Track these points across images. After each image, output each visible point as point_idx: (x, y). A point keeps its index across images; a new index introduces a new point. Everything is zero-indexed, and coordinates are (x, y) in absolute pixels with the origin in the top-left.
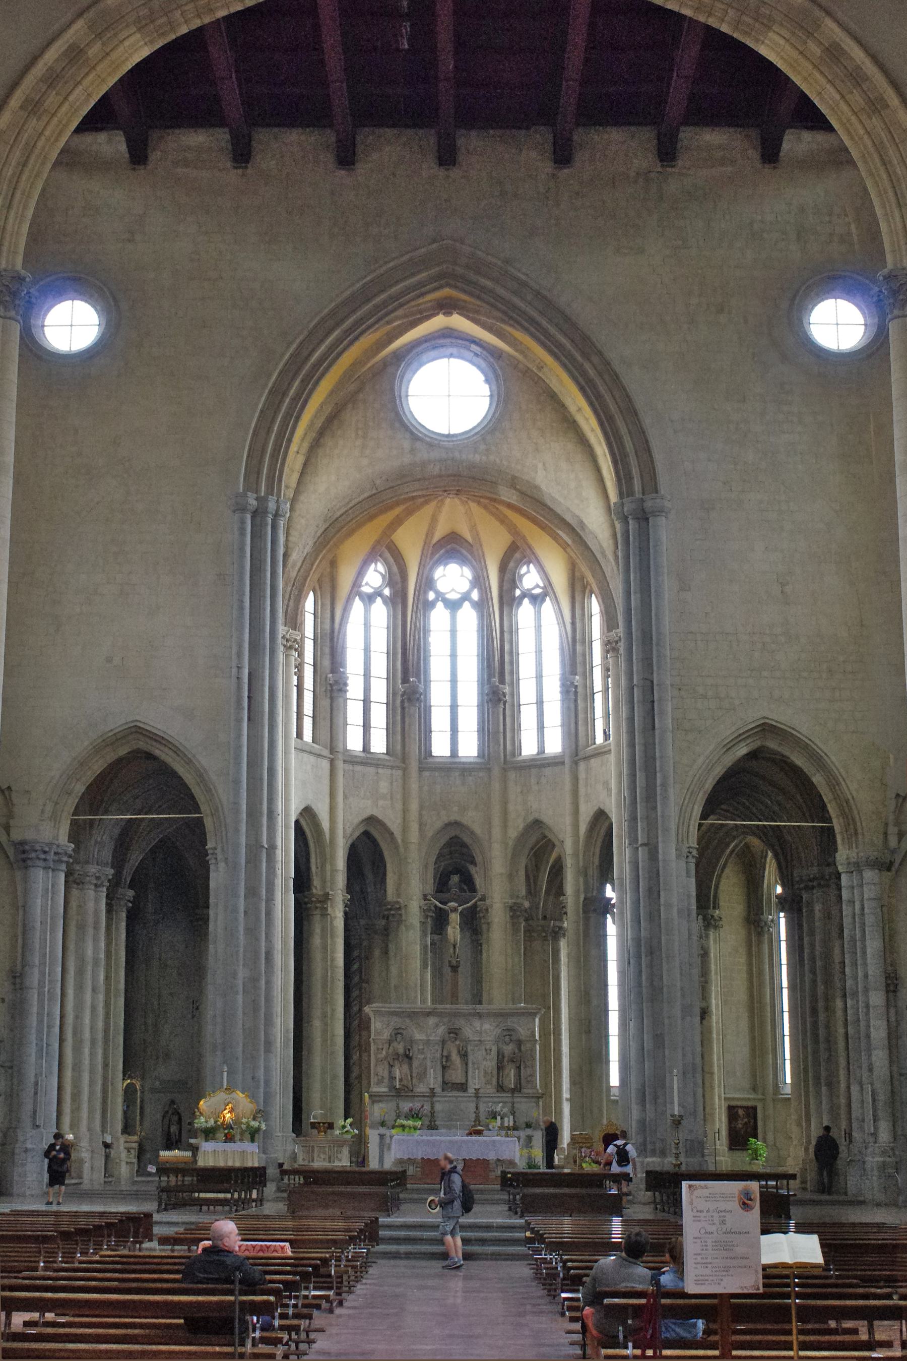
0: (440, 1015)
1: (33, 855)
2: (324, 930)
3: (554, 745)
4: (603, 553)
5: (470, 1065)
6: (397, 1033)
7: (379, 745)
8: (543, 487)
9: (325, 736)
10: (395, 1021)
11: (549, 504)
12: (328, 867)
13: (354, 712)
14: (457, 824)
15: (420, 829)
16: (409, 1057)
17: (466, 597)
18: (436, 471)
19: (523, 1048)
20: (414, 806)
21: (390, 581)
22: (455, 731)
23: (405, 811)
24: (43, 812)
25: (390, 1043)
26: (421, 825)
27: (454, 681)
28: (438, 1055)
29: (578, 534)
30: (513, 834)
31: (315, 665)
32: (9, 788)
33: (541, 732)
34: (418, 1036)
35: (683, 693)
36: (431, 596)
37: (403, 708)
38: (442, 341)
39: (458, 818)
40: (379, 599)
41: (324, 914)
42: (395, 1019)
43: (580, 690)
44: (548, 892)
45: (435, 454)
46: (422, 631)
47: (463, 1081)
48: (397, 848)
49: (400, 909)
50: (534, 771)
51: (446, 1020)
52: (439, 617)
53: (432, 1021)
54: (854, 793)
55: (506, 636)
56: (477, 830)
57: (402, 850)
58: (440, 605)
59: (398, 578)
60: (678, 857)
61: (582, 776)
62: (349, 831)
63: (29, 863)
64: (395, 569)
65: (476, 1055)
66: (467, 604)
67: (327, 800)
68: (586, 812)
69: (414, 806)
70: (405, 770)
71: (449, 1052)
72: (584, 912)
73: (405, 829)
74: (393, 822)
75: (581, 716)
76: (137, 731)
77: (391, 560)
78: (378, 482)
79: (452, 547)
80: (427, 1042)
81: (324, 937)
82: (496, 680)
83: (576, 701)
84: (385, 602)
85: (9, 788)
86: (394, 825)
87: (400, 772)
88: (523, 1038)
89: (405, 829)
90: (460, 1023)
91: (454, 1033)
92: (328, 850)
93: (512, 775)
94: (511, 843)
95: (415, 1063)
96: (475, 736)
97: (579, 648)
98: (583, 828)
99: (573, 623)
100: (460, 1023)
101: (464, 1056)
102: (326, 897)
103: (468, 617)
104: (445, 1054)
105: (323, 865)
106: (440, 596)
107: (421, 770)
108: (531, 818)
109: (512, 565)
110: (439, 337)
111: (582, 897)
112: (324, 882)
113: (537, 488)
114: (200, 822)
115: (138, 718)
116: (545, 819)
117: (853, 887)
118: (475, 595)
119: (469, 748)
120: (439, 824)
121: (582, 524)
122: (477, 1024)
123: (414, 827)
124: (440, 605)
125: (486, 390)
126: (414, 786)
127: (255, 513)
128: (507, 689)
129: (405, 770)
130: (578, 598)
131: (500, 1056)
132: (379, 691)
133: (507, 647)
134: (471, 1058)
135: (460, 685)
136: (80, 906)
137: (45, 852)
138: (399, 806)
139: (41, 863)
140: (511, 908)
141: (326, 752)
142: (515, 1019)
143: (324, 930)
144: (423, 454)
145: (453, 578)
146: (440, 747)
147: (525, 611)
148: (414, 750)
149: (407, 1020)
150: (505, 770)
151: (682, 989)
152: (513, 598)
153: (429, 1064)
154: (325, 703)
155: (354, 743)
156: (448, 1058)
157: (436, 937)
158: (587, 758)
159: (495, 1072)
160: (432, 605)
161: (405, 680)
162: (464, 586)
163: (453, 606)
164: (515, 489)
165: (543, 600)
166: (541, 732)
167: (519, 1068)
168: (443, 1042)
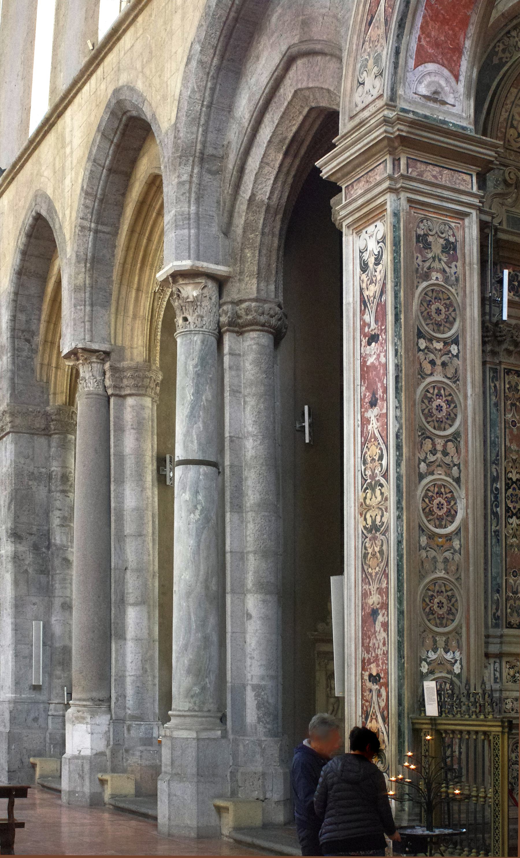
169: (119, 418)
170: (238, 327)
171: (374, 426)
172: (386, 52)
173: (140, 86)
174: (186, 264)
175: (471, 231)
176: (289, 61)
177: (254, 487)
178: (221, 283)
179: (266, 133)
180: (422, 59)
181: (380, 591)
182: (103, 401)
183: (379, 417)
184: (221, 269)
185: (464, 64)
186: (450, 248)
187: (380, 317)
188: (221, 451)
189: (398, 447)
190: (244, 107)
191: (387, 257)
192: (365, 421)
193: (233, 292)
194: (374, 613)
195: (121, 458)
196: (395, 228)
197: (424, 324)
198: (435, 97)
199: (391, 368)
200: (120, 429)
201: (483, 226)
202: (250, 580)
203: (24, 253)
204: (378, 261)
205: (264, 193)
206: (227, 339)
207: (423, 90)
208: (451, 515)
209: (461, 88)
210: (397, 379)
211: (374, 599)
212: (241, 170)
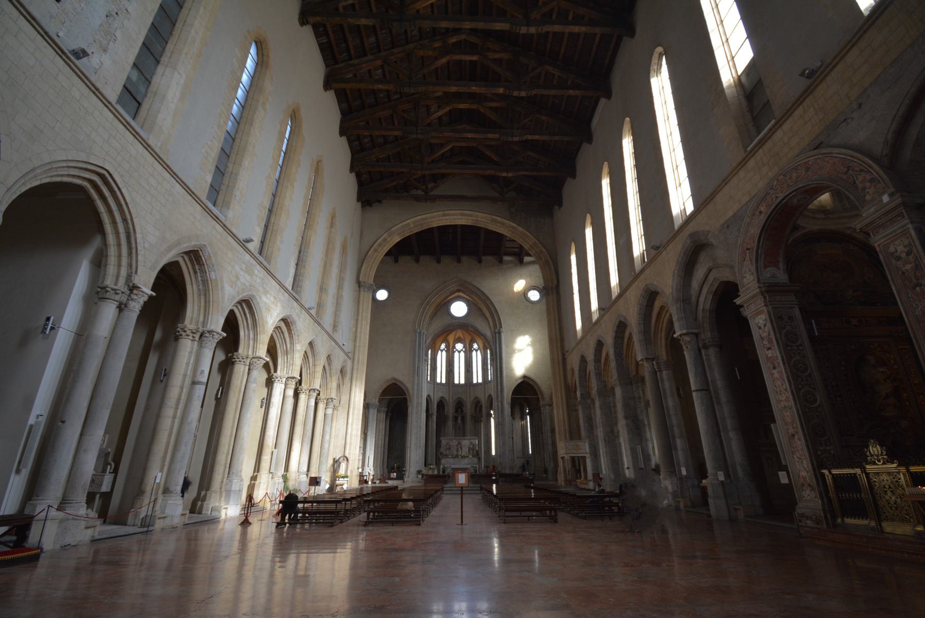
6: (447, 444)
22: (459, 378)
52: (456, 354)
74: (446, 397)
79: (459, 340)
91: (459, 443)
103: (462, 354)
119: (463, 382)
145: (459, 346)
146: (456, 382)
163: (459, 352)
166: (478, 378)
169: (661, 378)
170: (706, 347)
171: (776, 375)
172: (753, 269)
173: (655, 283)
174: (685, 331)
175: (797, 312)
176: (710, 270)
177: (723, 397)
178: (697, 335)
179: (705, 291)
180: (766, 267)
181: (793, 428)
182: (654, 373)
183: (778, 372)
184: (696, 331)
185: (781, 265)
186: (791, 318)
187: (770, 341)
188: (708, 384)
189: (789, 381)
190: (695, 284)
191: (769, 325)
192: (772, 374)
193: (702, 336)
194: (793, 435)
195: (664, 390)
196: (770, 316)
197: (788, 343)
198: (773, 276)
199: (779, 357)
200: (662, 381)
201: (800, 308)
202: (729, 427)
203: (616, 332)
204: (765, 325)
205: (708, 307)
206: (703, 351)
207: (768, 275)
208: (816, 401)
209: (781, 271)
210: (783, 360)
211: (791, 431)
212: (698, 301)
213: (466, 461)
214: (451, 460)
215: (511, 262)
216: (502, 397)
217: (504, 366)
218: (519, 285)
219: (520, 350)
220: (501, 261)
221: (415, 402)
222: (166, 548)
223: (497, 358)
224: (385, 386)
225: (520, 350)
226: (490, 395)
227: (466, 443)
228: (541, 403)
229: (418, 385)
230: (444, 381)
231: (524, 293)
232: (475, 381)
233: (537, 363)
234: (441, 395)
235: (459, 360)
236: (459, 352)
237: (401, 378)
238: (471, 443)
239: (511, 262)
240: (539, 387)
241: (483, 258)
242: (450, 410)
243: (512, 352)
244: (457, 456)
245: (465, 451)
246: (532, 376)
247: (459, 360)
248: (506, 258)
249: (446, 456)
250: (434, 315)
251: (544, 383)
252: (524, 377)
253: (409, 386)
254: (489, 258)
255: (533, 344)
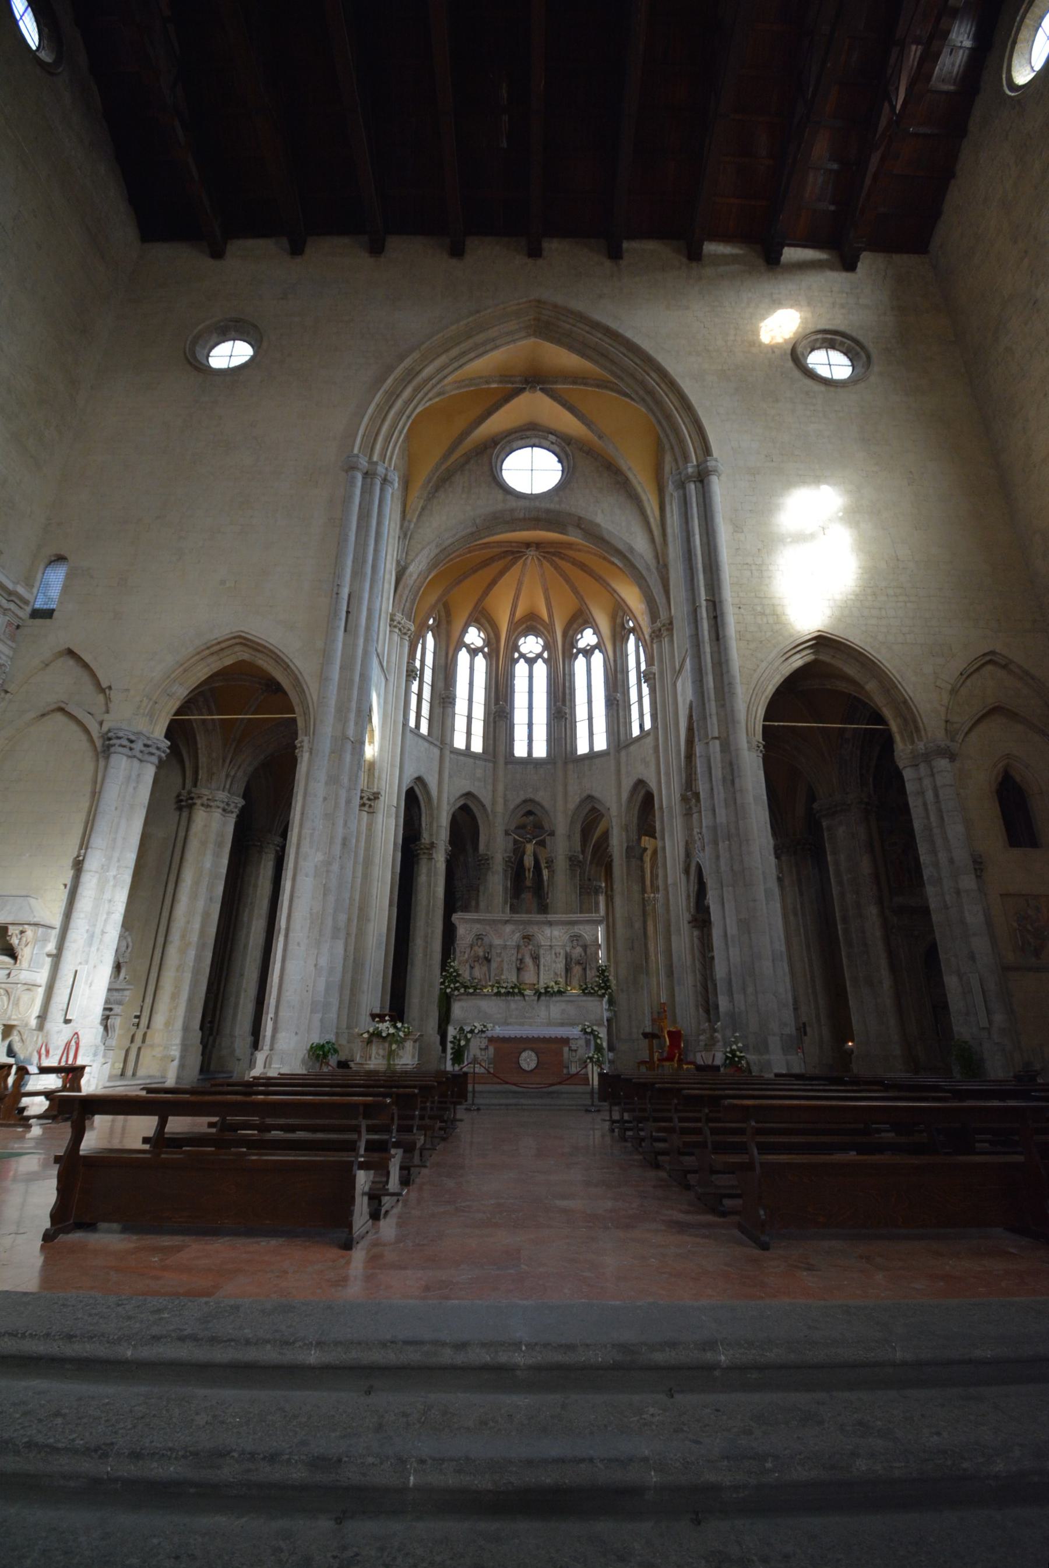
0: (516, 922)
1: (118, 742)
2: (429, 870)
3: (601, 744)
4: (648, 569)
5: (542, 967)
6: (479, 937)
7: (477, 746)
8: (602, 524)
9: (437, 732)
10: (477, 928)
11: (607, 537)
12: (435, 825)
13: (460, 723)
14: (531, 801)
15: (505, 804)
16: (488, 960)
17: (540, 656)
18: (522, 515)
19: (588, 952)
20: (501, 788)
21: (488, 642)
22: (530, 739)
23: (494, 791)
24: (139, 707)
25: (471, 946)
26: (506, 801)
27: (530, 725)
28: (514, 958)
29: (628, 560)
30: (572, 806)
31: (432, 686)
32: (110, 688)
33: (591, 735)
34: (497, 942)
35: (742, 610)
36: (516, 655)
37: (495, 722)
38: (528, 433)
39: (532, 796)
40: (480, 654)
41: (431, 859)
42: (478, 926)
43: (621, 703)
44: (591, 863)
45: (522, 503)
46: (510, 676)
47: (535, 982)
48: (487, 817)
49: (487, 859)
50: (587, 762)
51: (521, 927)
52: (521, 669)
53: (509, 928)
54: (911, 694)
55: (567, 677)
56: (546, 804)
57: (491, 818)
58: (522, 660)
59: (494, 641)
60: (749, 749)
61: (623, 759)
62: (452, 800)
63: (112, 749)
64: (492, 635)
65: (546, 959)
66: (540, 661)
67: (436, 776)
68: (627, 784)
69: (501, 788)
70: (495, 763)
71: (523, 955)
72: (627, 857)
73: (494, 803)
74: (485, 797)
75: (622, 720)
76: (244, 641)
77: (489, 629)
78: (478, 521)
79: (530, 624)
80: (505, 947)
81: (429, 875)
82: (559, 704)
83: (618, 710)
84: (485, 657)
85: (110, 688)
86: (486, 800)
87: (491, 765)
88: (589, 943)
89: (494, 803)
90: (533, 930)
91: (528, 938)
92: (435, 812)
93: (571, 766)
94: (570, 813)
95: (494, 965)
96: (545, 744)
97: (619, 676)
98: (625, 796)
99: (615, 661)
100: (533, 930)
101: (536, 958)
102: (432, 845)
103: (541, 669)
104: (520, 957)
105: (431, 823)
106: (522, 656)
107: (506, 763)
108: (585, 795)
109: (571, 632)
110: (528, 429)
111: (625, 846)
112: (431, 835)
113: (598, 525)
114: (294, 720)
115: (242, 629)
116: (596, 794)
117: (920, 779)
118: (545, 655)
119: (540, 751)
120: (518, 801)
121: (631, 549)
122: (547, 931)
123: (500, 801)
124: (522, 660)
125: (559, 466)
126: (501, 773)
127: (366, 474)
128: (567, 711)
129: (495, 763)
130: (618, 644)
131: (568, 957)
132: (479, 712)
133: (567, 684)
134: (542, 961)
135: (534, 743)
136: (205, 826)
137: (132, 742)
138: (490, 787)
139: (126, 751)
140: (570, 859)
141: (438, 744)
142: (581, 927)
143: (429, 870)
144: (512, 503)
145: (531, 645)
146: (520, 750)
147: (580, 662)
148: (501, 749)
149: (488, 928)
150: (566, 763)
151: (763, 873)
152: (572, 654)
153: (505, 966)
154: (438, 710)
155: (459, 743)
156: (521, 961)
157: (515, 901)
158: (627, 746)
159: (563, 974)
160: (517, 661)
161: (497, 703)
162: (538, 649)
163: (531, 662)
164: (581, 529)
165: (592, 653)
166: (591, 735)
167: (585, 969)
168: (518, 947)
213: (556, 1009)
214: (491, 1006)
215: (734, 259)
216: (727, 718)
217: (729, 595)
218: (780, 325)
219: (801, 538)
220: (694, 255)
221: (327, 729)
222: (16, 1146)
223: (690, 600)
224: (202, 673)
225: (801, 538)
226: (640, 783)
227: (553, 937)
228: (902, 749)
229: (347, 666)
230: (477, 746)
231: (795, 356)
232: (582, 748)
233: (877, 586)
234: (464, 785)
235: (530, 686)
236: (531, 662)
237: (267, 630)
238: (576, 938)
239: (734, 259)
240: (888, 685)
241: (625, 245)
242: (496, 842)
243: (768, 542)
244: (515, 991)
245: (550, 970)
246: (856, 638)
247: (530, 686)
248: (711, 248)
249: (473, 990)
250: (442, 481)
251: (919, 672)
252: (821, 642)
253: (304, 665)
254: (651, 245)
255: (852, 515)
